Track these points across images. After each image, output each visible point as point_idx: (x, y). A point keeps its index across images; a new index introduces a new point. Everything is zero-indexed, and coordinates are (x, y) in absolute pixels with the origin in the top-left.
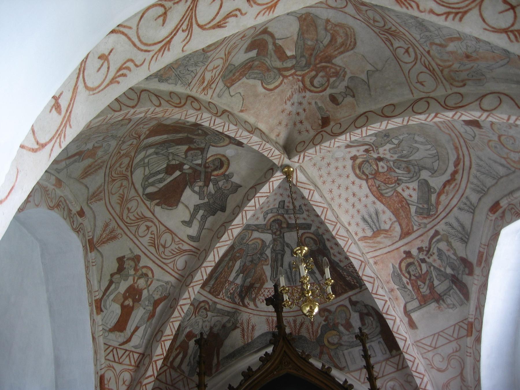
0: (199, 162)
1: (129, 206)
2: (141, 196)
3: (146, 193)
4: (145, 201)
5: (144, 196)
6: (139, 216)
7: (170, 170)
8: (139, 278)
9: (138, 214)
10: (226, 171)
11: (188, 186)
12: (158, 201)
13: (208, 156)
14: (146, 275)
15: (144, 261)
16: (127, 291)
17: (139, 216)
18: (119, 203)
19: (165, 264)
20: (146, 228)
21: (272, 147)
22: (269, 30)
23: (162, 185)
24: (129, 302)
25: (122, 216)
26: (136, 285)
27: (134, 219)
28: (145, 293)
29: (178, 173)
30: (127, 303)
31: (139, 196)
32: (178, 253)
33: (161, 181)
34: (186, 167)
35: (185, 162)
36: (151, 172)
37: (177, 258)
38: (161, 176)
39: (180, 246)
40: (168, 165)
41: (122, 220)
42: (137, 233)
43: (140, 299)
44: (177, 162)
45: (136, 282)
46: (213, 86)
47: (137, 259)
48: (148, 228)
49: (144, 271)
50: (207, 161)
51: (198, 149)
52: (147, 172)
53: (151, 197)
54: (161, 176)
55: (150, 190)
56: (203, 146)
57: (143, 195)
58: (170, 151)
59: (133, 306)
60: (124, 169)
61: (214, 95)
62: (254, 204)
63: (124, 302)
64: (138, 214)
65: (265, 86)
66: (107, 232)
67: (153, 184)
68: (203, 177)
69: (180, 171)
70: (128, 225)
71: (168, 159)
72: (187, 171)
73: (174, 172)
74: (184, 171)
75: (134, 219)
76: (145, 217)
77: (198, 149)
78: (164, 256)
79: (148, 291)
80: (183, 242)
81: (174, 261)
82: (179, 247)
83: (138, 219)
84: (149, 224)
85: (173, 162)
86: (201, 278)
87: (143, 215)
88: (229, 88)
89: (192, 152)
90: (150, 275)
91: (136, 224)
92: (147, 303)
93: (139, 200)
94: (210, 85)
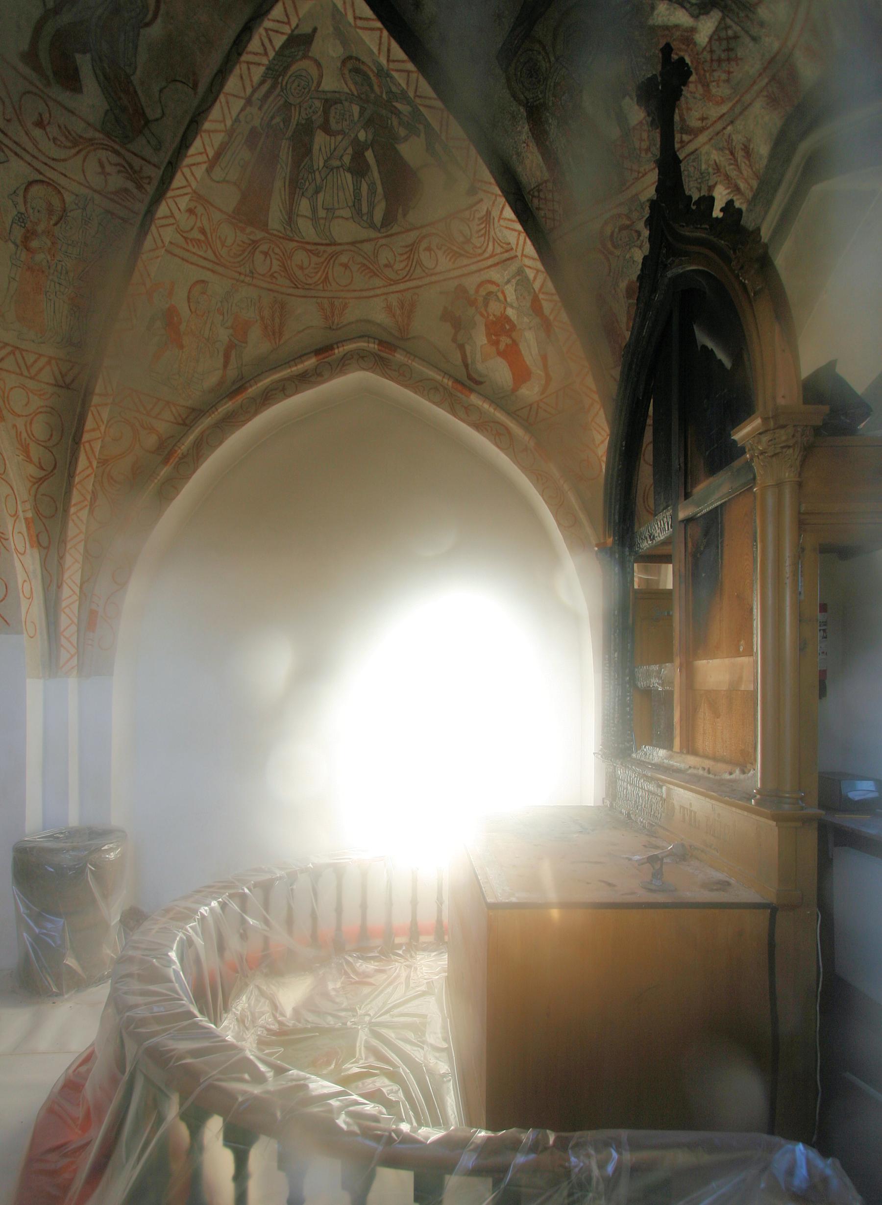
0: (356, 109)
1: (383, 261)
2: (380, 235)
3: (379, 225)
4: (389, 233)
5: (382, 230)
6: (406, 253)
7: (359, 169)
8: (486, 305)
9: (401, 255)
10: (372, 70)
11: (396, 146)
12: (400, 211)
13: (346, 90)
14: (490, 293)
15: (471, 283)
16: (488, 335)
17: (406, 253)
18: (371, 277)
19: (491, 256)
20: (428, 253)
21: (261, 30)
22: (25, 46)
23: (380, 189)
24: (505, 341)
25: (391, 280)
26: (491, 317)
27: (405, 263)
28: (510, 312)
29: (369, 155)
30: (502, 346)
31: (378, 238)
32: (485, 227)
33: (372, 191)
34: (362, 136)
35: (353, 135)
36: (350, 204)
37: (492, 233)
38: (364, 188)
39: (478, 216)
40: (349, 170)
41: (396, 282)
42: (427, 271)
43: (513, 327)
44: (350, 151)
45: (488, 314)
46: (137, 163)
47: (461, 290)
48: (428, 249)
49: (483, 292)
50: (356, 93)
51: (326, 112)
52: (346, 213)
53: (389, 220)
54: (364, 188)
55: (378, 215)
56: (318, 104)
57: (379, 231)
58: (321, 164)
59: (514, 341)
60: (314, 259)
61: (155, 160)
62: (405, 75)
63: (497, 349)
64: (401, 255)
65: (150, 16)
66: (398, 312)
67: (372, 206)
68: (384, 112)
69: (367, 149)
70: (408, 277)
71: (338, 168)
72: (370, 137)
73: (366, 162)
74: (369, 142)
75: (405, 263)
76: (413, 244)
77: (326, 112)
78: (480, 251)
79: (512, 307)
80: (474, 208)
81: (494, 239)
82: (479, 219)
83: (409, 258)
84: (424, 245)
85: (347, 159)
86: (516, 234)
87: (407, 247)
88: (147, 122)
89: (332, 121)
90: (493, 288)
91: (414, 264)
92: (526, 320)
93: (383, 241)
94: (135, 172)
